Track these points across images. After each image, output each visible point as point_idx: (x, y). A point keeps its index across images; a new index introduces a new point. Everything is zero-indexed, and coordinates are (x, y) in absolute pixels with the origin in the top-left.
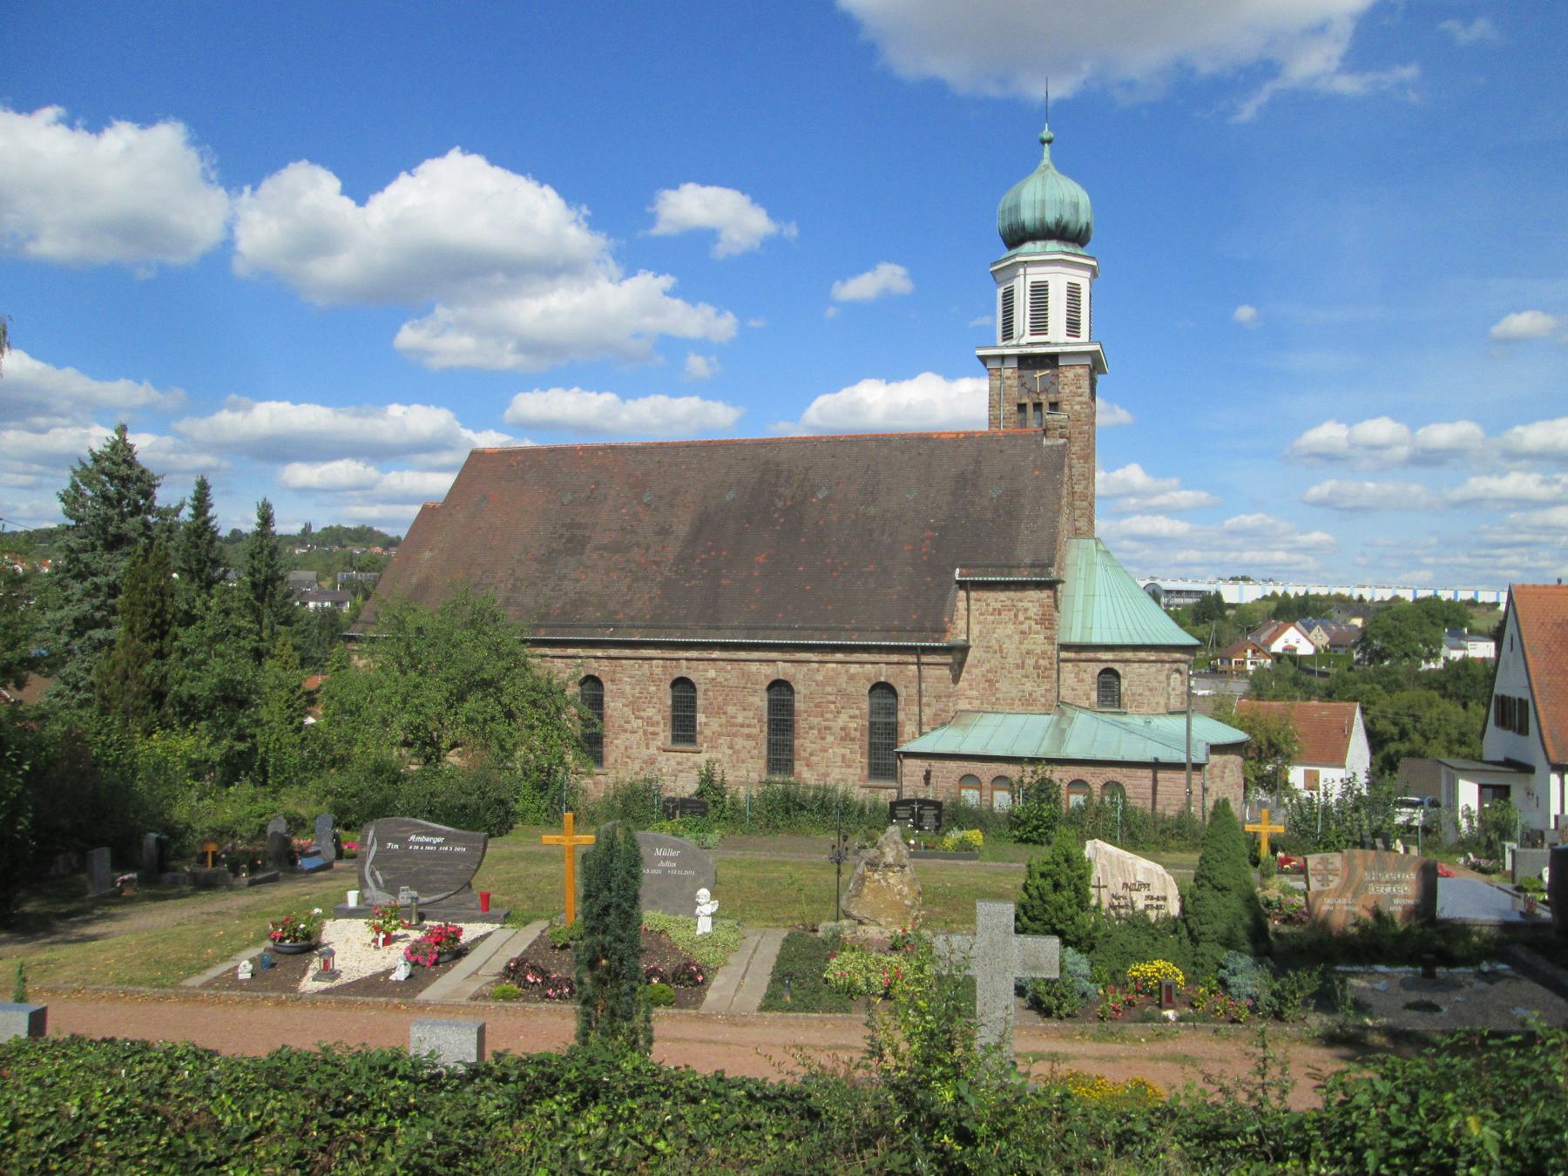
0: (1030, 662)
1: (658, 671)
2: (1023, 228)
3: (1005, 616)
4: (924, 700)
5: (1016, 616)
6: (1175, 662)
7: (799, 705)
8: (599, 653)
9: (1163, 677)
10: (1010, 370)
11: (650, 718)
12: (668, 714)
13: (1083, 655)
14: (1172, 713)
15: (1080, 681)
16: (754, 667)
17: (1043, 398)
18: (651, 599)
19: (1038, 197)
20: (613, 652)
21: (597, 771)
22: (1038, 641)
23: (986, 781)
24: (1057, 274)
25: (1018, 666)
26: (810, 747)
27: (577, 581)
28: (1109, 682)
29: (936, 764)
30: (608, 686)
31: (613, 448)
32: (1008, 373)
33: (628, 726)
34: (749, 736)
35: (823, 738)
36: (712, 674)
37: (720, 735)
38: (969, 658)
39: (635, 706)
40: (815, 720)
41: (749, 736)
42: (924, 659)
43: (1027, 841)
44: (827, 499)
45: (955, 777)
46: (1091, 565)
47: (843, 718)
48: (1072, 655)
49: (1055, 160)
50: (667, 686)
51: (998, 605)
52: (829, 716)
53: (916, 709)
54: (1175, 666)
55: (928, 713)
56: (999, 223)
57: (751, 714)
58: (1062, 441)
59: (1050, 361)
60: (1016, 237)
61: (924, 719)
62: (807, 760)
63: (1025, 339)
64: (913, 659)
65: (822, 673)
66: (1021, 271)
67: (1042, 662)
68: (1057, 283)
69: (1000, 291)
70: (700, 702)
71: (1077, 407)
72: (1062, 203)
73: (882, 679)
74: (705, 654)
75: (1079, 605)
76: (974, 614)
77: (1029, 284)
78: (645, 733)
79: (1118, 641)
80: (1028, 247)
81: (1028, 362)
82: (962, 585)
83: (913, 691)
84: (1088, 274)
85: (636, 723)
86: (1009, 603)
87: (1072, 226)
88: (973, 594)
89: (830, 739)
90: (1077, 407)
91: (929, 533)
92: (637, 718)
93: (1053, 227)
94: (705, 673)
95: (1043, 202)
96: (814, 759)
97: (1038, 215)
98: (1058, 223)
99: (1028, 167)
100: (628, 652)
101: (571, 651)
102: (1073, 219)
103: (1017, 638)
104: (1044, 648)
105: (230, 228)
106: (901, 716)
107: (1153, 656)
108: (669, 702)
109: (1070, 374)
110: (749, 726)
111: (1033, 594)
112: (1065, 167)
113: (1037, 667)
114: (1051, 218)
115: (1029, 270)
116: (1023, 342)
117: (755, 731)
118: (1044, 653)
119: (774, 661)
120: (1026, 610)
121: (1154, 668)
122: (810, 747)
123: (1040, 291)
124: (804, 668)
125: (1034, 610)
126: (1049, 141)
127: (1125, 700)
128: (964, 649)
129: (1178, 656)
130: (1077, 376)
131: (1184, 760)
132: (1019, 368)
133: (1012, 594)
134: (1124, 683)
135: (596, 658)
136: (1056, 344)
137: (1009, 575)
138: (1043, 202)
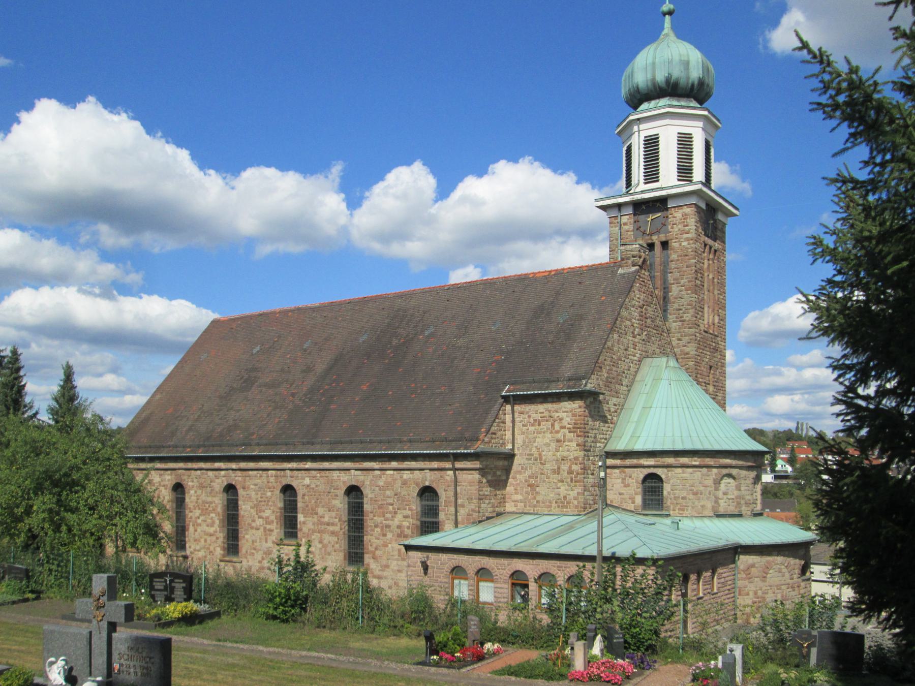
0: (565, 467)
1: (272, 479)
2: (638, 90)
3: (545, 425)
4: (459, 501)
5: (553, 425)
6: (726, 467)
7: (367, 507)
8: (234, 466)
9: (709, 482)
10: (627, 218)
11: (268, 518)
12: (345, 517)
13: (628, 462)
14: (718, 516)
15: (625, 486)
16: (336, 474)
17: (655, 238)
18: (280, 422)
19: (650, 61)
20: (243, 465)
21: (235, 559)
22: (572, 449)
23: (471, 572)
24: (669, 127)
25: (554, 472)
26: (376, 542)
27: (238, 411)
28: (652, 486)
29: (433, 556)
30: (241, 492)
31: (299, 309)
32: (625, 219)
33: (254, 524)
34: (333, 533)
35: (385, 535)
36: (307, 481)
37: (314, 531)
38: (515, 467)
39: (258, 508)
40: (378, 520)
41: (333, 533)
42: (458, 465)
43: (274, 618)
44: (432, 335)
45: (447, 567)
46: (657, 380)
47: (399, 517)
48: (617, 462)
49: (674, 28)
50: (277, 492)
51: (538, 417)
52: (388, 516)
53: (453, 509)
54: (725, 471)
55: (462, 512)
56: (624, 91)
57: (334, 514)
58: (634, 269)
59: (659, 204)
60: (637, 98)
61: (460, 518)
62: (374, 553)
63: (642, 190)
64: (448, 465)
65: (384, 478)
66: (636, 128)
67: (574, 467)
68: (668, 136)
69: (625, 148)
70: (300, 505)
71: (685, 244)
72: (670, 62)
73: (427, 484)
74: (302, 465)
75: (635, 417)
76: (518, 425)
77: (642, 138)
78: (265, 528)
79: (658, 447)
80: (645, 106)
81: (642, 207)
82: (506, 399)
83: (451, 493)
84: (701, 124)
85: (259, 522)
86: (546, 414)
87: (682, 82)
88: (517, 408)
89: (389, 536)
90: (685, 244)
91: (498, 357)
92: (260, 517)
93: (663, 85)
94: (305, 481)
95: (654, 64)
96: (378, 553)
97: (649, 76)
98: (668, 80)
99: (653, 36)
100: (251, 465)
101: (217, 465)
102: (683, 75)
103: (553, 445)
104: (576, 454)
105: (351, 215)
106: (442, 516)
107: (696, 461)
108: (281, 505)
109: (678, 214)
110: (333, 524)
111: (567, 405)
112: (682, 33)
113: (570, 472)
114: (660, 77)
115: (642, 127)
116: (638, 190)
117: (337, 528)
118: (576, 458)
119: (349, 470)
120: (561, 420)
121: (698, 474)
122: (376, 542)
123: (652, 143)
124: (370, 475)
125: (567, 420)
126: (670, 13)
127: (668, 503)
128: (510, 457)
129: (727, 461)
130: (685, 216)
131: (595, 553)
132: (635, 214)
133: (549, 406)
134: (667, 488)
135: (233, 470)
136: (662, 189)
137: (547, 388)
138: (654, 64)
